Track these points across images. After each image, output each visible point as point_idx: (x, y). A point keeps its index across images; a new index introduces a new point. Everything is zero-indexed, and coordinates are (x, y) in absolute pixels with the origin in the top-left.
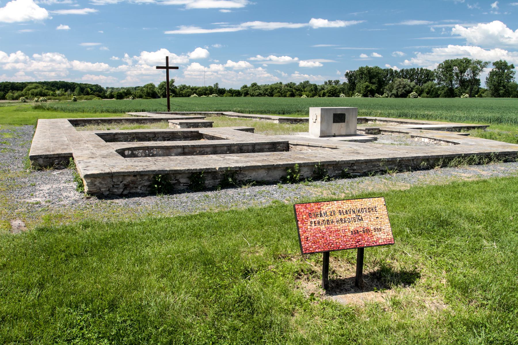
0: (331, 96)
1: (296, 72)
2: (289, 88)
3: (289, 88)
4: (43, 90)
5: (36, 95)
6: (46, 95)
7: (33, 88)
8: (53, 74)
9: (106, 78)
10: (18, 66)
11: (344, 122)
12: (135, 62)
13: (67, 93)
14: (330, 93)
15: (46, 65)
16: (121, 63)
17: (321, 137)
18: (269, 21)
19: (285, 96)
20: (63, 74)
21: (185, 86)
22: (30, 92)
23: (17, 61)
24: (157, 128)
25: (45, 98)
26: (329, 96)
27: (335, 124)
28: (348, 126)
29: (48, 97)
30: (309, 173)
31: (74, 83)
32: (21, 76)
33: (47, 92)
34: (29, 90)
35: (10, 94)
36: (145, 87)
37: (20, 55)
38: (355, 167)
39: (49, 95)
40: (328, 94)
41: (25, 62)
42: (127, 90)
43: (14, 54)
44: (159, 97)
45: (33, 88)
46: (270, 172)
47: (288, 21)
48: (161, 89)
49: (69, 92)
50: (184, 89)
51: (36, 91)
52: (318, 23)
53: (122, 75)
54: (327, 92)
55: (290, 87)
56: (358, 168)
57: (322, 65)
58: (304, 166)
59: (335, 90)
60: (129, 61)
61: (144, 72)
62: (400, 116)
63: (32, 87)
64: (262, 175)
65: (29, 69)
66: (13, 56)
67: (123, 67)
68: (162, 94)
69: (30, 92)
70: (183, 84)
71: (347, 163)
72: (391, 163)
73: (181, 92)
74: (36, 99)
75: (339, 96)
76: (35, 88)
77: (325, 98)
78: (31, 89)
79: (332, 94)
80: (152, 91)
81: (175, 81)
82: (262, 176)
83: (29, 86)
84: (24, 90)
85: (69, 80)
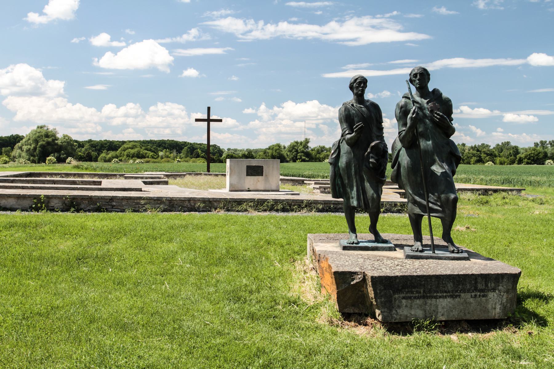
0: (531, 164)
1: (499, 129)
2: (475, 152)
3: (475, 152)
4: (142, 150)
5: (133, 156)
6: (145, 158)
7: (130, 148)
8: (167, 131)
9: (230, 136)
10: (130, 121)
11: (262, 175)
12: (274, 116)
13: (172, 155)
14: (529, 159)
15: (161, 120)
16: (254, 117)
17: (231, 191)
18: (476, 58)
19: (469, 163)
20: (179, 132)
21: (324, 147)
22: (125, 153)
23: (127, 116)
24: (239, 195)
25: (142, 160)
26: (528, 163)
27: (249, 177)
28: (267, 180)
29: (147, 159)
30: (60, 204)
31: (185, 142)
32: (130, 133)
33: (146, 153)
34: (124, 151)
35: (103, 155)
36: (269, 148)
37: (131, 108)
38: (114, 204)
39: (148, 157)
40: (526, 160)
41: (136, 116)
42: (249, 153)
44: (287, 162)
45: (130, 148)
46: (19, 201)
47: (506, 57)
48: (290, 151)
49: (175, 154)
50: (322, 151)
51: (132, 151)
52: (539, 59)
53: (253, 134)
54: (526, 157)
55: (478, 151)
56: (117, 204)
57: (536, 119)
58: (55, 198)
59: (537, 155)
60: (265, 116)
61: (283, 129)
62: (503, 183)
63: (128, 146)
64: (11, 202)
65: (141, 125)
66: (123, 110)
67: (256, 123)
68: (293, 158)
69: (125, 153)
70: (322, 145)
71: (104, 199)
72: (159, 202)
73: (318, 156)
74: (131, 161)
75: (543, 164)
76: (132, 148)
77: (522, 165)
78: (128, 148)
79: (533, 160)
80: (279, 153)
81: (310, 140)
82: (11, 203)
83: (125, 146)
84: (120, 150)
85: (180, 139)
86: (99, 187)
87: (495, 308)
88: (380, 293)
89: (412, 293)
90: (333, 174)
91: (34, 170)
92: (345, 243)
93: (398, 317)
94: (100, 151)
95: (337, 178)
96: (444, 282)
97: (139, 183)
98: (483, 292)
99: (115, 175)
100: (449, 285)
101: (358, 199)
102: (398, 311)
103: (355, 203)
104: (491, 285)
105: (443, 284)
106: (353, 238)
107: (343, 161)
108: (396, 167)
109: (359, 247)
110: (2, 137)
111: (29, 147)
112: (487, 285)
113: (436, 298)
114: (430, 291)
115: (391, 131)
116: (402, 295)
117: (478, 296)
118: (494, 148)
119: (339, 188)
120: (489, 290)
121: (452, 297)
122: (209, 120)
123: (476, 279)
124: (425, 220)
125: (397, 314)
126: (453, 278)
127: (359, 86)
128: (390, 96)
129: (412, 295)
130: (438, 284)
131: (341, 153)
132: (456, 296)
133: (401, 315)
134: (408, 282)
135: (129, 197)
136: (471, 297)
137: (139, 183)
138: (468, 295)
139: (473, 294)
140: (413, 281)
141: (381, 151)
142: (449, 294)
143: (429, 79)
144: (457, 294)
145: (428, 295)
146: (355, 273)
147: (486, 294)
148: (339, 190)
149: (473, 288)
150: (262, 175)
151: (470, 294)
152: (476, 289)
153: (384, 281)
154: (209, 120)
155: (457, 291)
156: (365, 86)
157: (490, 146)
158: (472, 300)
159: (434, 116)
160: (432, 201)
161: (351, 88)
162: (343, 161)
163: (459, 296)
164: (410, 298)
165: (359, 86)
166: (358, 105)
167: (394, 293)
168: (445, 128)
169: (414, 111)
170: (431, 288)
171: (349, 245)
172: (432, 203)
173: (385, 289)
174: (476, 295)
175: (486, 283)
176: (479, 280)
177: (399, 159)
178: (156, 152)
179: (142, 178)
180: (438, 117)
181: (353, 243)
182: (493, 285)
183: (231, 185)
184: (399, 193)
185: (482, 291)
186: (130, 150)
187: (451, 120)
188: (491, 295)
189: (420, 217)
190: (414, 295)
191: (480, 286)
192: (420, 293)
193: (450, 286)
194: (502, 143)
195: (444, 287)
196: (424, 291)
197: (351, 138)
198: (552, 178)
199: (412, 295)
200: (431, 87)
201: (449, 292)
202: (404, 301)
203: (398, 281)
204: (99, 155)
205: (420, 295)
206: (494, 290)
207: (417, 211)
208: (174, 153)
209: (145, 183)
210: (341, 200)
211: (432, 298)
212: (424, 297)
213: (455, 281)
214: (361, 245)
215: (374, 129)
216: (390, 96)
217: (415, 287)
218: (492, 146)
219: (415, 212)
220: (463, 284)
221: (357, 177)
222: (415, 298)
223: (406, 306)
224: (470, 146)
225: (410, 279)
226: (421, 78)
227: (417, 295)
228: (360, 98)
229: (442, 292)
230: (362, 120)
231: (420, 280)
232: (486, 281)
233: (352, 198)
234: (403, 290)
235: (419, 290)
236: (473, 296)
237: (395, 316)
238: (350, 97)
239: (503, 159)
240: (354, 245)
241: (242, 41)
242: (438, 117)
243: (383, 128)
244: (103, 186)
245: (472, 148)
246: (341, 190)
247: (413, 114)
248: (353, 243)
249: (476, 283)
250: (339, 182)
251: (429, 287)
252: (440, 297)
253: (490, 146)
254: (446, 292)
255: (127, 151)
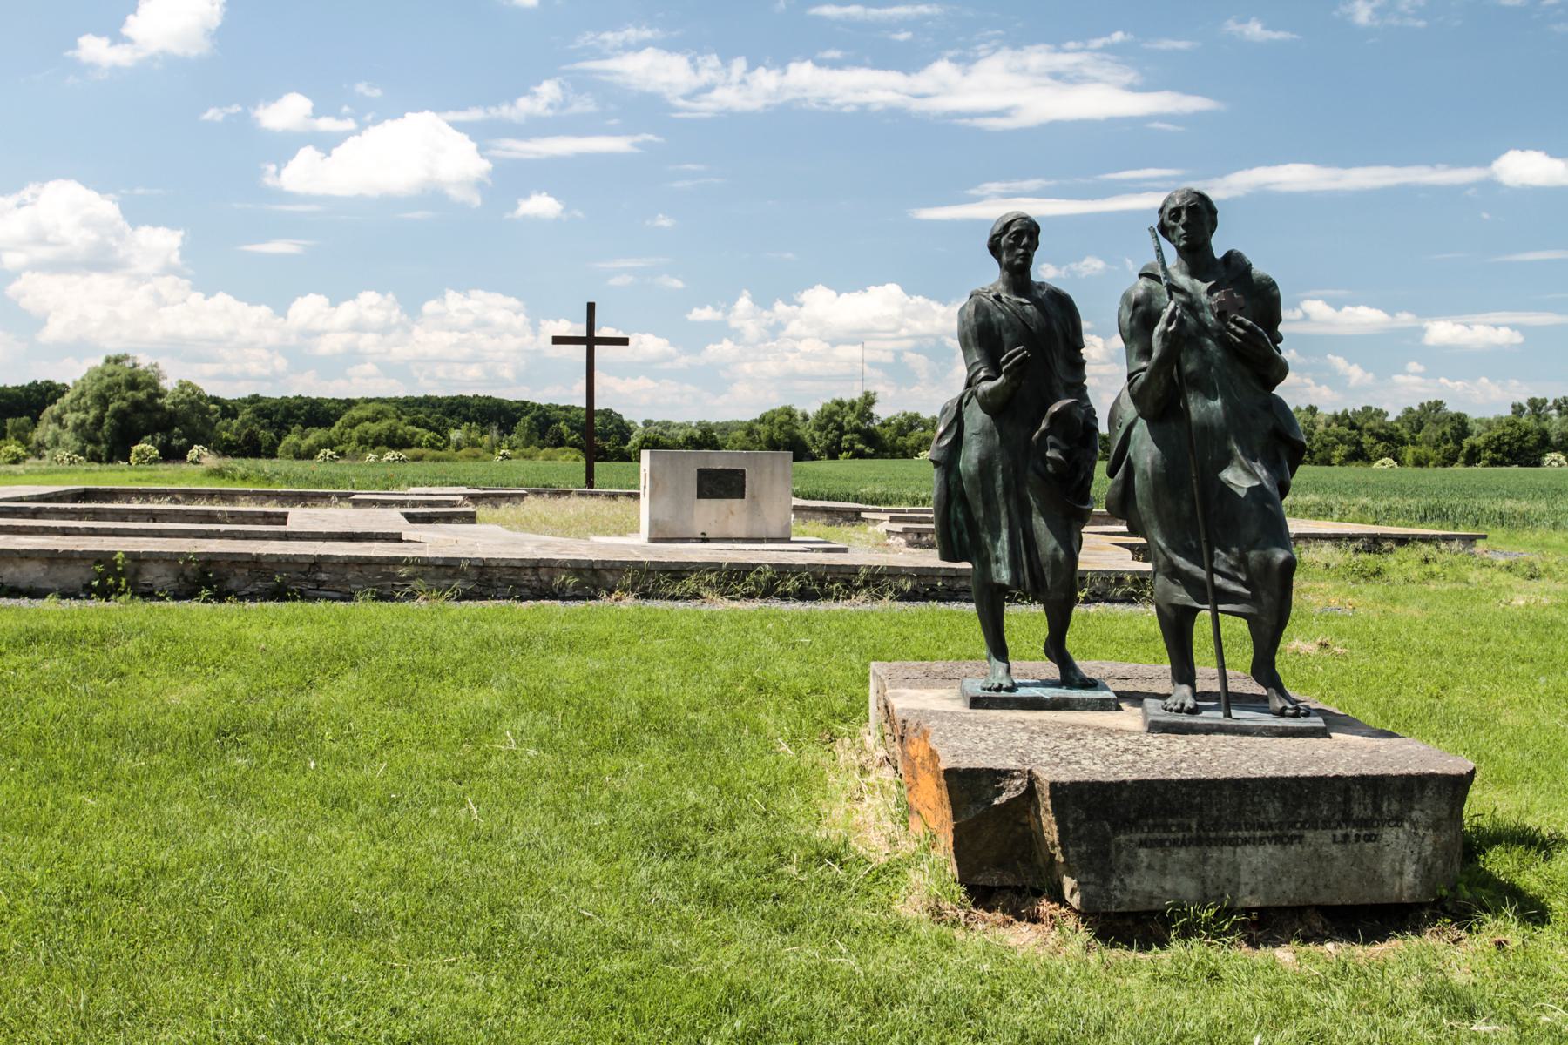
0: (1502, 463)
1: (1413, 366)
2: (1344, 430)
3: (1344, 430)
4: (401, 424)
5: (376, 442)
6: (409, 446)
7: (368, 419)
8: (474, 371)
9: (650, 384)
10: (368, 341)
11: (743, 497)
12: (776, 330)
13: (486, 438)
14: (1497, 450)
15: (454, 341)
16: (720, 331)
17: (653, 540)
18: (1347, 164)
19: (1327, 462)
20: (507, 373)
21: (917, 416)
22: (355, 433)
23: (358, 327)
25: (403, 454)
26: (1493, 462)
27: (704, 501)
28: (755, 508)
29: (415, 451)
30: (170, 579)
31: (525, 403)
32: (367, 377)
33: (414, 435)
34: (352, 426)
35: (291, 439)
36: (762, 420)
37: (370, 305)
38: (323, 576)
39: (419, 445)
40: (1488, 454)
41: (385, 330)
42: (704, 432)
43: (459, 296)
44: (813, 458)
45: (368, 419)
46: (54, 568)
47: (1431, 162)
48: (821, 428)
49: (496, 436)
50: (912, 428)
51: (374, 428)
52: (1525, 167)
53: (715, 378)
54: (1488, 445)
55: (1353, 426)
56: (333, 578)
57: (1518, 338)
58: (156, 561)
59: (1521, 438)
60: (751, 329)
61: (802, 367)
62: (1423, 519)
63: (363, 414)
64: (32, 573)
65: (399, 353)
66: (347, 311)
67: (725, 348)
68: (828, 448)
69: (355, 433)
70: (910, 411)
71: (296, 563)
72: (450, 572)
73: (899, 441)
74: (371, 456)
75: (1538, 464)
76: (374, 420)
77: (1478, 469)
78: (361, 420)
79: (1508, 454)
80: (790, 434)
81: (878, 397)
82: (32, 576)
83: (355, 413)
84: (339, 423)
85: (510, 394)
86: (281, 528)
87: (1401, 874)
88: (1076, 830)
89: (1167, 828)
90: (944, 493)
91: (96, 480)
92: (976, 688)
93: (1127, 898)
94: (282, 429)
95: (954, 503)
96: (1256, 799)
97: (392, 520)
98: (1367, 827)
99: (325, 497)
100: (1270, 808)
101: (1014, 564)
102: (1127, 881)
103: (1004, 575)
104: (1391, 806)
105: (1253, 803)
106: (998, 673)
107: (970, 457)
108: (1120, 474)
109: (1017, 699)
110: (5, 388)
111: (82, 416)
112: (1377, 808)
113: (1234, 843)
114: (1217, 825)
115: (1107, 371)
116: (1137, 836)
117: (1353, 838)
118: (1398, 419)
119: (960, 533)
120: (1383, 823)
121: (1278, 840)
122: (590, 341)
123: (1347, 790)
124: (1202, 624)
125: (1124, 889)
126: (1283, 786)
127: (1016, 242)
128: (1103, 272)
129: (1165, 836)
130: (1241, 804)
131: (966, 434)
132: (1291, 839)
133: (1134, 893)
134: (1156, 799)
135: (366, 558)
136: (1334, 841)
137: (392, 520)
138: (1325, 836)
139: (1339, 832)
140: (1170, 795)
141: (1078, 429)
142: (1270, 833)
143: (1214, 224)
144: (1294, 832)
145: (1212, 835)
146: (1006, 774)
147: (1375, 831)
148: (960, 539)
149: (1338, 816)
150: (743, 497)
151: (1329, 833)
152: (1347, 819)
153: (1086, 797)
154: (590, 341)
155: (1292, 825)
156: (1034, 244)
157: (1387, 414)
158: (1335, 850)
159: (1228, 327)
160: (1223, 568)
161: (994, 248)
162: (970, 457)
163: (1300, 838)
164: (1160, 843)
165: (1016, 242)
166: (1015, 299)
167: (1114, 830)
168: (1259, 361)
169: (1173, 314)
170: (1220, 817)
171: (987, 694)
172: (1223, 575)
173: (1090, 818)
174: (1346, 837)
175: (1374, 803)
176: (1356, 793)
177: (1131, 451)
178: (440, 430)
179: (402, 504)
180: (1241, 331)
181: (998, 689)
182: (1395, 806)
183: (654, 524)
184: (1130, 547)
185: (1363, 823)
186: (367, 424)
187: (1278, 339)
188: (1389, 835)
189: (1189, 614)
190: (1172, 836)
191: (1358, 811)
192: (1189, 828)
193: (1273, 810)
194: (1422, 405)
195: (1258, 813)
196: (1200, 825)
197: (993, 392)
198: (1563, 504)
199: (1165, 836)
200: (1220, 245)
201: (1271, 826)
202: (1143, 853)
203: (1125, 794)
204: (280, 439)
205: (1188, 835)
206: (1398, 821)
207: (1182, 596)
208: (494, 434)
209: (411, 518)
210: (966, 565)
211: (1224, 843)
212: (1199, 841)
213: (1288, 796)
214: (1022, 692)
215: (1060, 366)
216: (1103, 272)
217: (1173, 814)
218: (1394, 413)
219: (1175, 601)
220: (1310, 805)
221: (1012, 502)
222: (1175, 843)
223: (1150, 867)
224: (1331, 412)
225: (1161, 789)
226: (1192, 221)
227: (1180, 835)
228: (1018, 276)
229: (1252, 826)
230: (1024, 340)
231: (1188, 794)
232: (1375, 796)
233: (997, 561)
234: (1141, 822)
235: (1186, 821)
236: (1339, 838)
237: (1118, 894)
238: (990, 275)
239: (1424, 450)
240: (1003, 694)
241: (686, 115)
242: (1241, 331)
243: (1083, 363)
244: (291, 526)
245: (1337, 419)
246: (966, 537)
247: (1169, 323)
248: (998, 689)
249: (1348, 801)
250: (960, 516)
251: (1215, 813)
252: (1246, 841)
253: (1387, 414)
254: (1261, 827)
255: (359, 428)
